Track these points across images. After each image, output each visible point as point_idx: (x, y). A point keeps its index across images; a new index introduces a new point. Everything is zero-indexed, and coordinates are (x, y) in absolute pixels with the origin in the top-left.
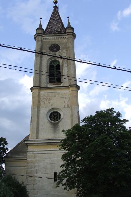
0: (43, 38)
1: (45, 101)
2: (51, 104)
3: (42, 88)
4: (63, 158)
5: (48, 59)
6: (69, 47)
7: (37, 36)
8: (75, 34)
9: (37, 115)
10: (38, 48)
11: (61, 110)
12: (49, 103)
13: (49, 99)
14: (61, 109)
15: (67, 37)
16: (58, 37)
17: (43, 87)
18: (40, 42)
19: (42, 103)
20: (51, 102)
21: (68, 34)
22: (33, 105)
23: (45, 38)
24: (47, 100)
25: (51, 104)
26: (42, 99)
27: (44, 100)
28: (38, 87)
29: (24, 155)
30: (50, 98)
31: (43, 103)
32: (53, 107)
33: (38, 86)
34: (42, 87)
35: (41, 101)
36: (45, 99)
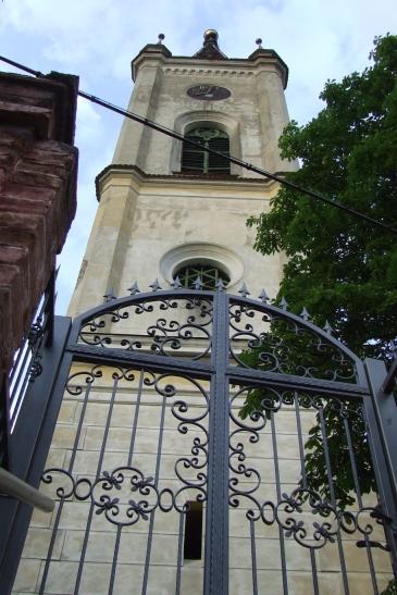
0: (164, 68)
1: (159, 221)
2: (183, 230)
3: (149, 176)
4: (323, 96)
5: (180, 113)
6: (265, 92)
7: (142, 61)
8: (285, 66)
9: (112, 254)
10: (144, 84)
11: (232, 252)
12: (177, 226)
13: (177, 214)
14: (233, 249)
15: (255, 72)
16: (222, 70)
17: (154, 176)
18: (155, 73)
19: (142, 225)
20: (186, 224)
21: (261, 63)
22: (102, 224)
23: (173, 69)
24: (169, 217)
25: (183, 230)
26: (144, 215)
27: (153, 215)
28: (133, 171)
29: (11, 196)
30: (183, 213)
31: (148, 224)
32: (192, 239)
33: (131, 167)
34: (147, 173)
35: (139, 217)
36: (158, 212)
